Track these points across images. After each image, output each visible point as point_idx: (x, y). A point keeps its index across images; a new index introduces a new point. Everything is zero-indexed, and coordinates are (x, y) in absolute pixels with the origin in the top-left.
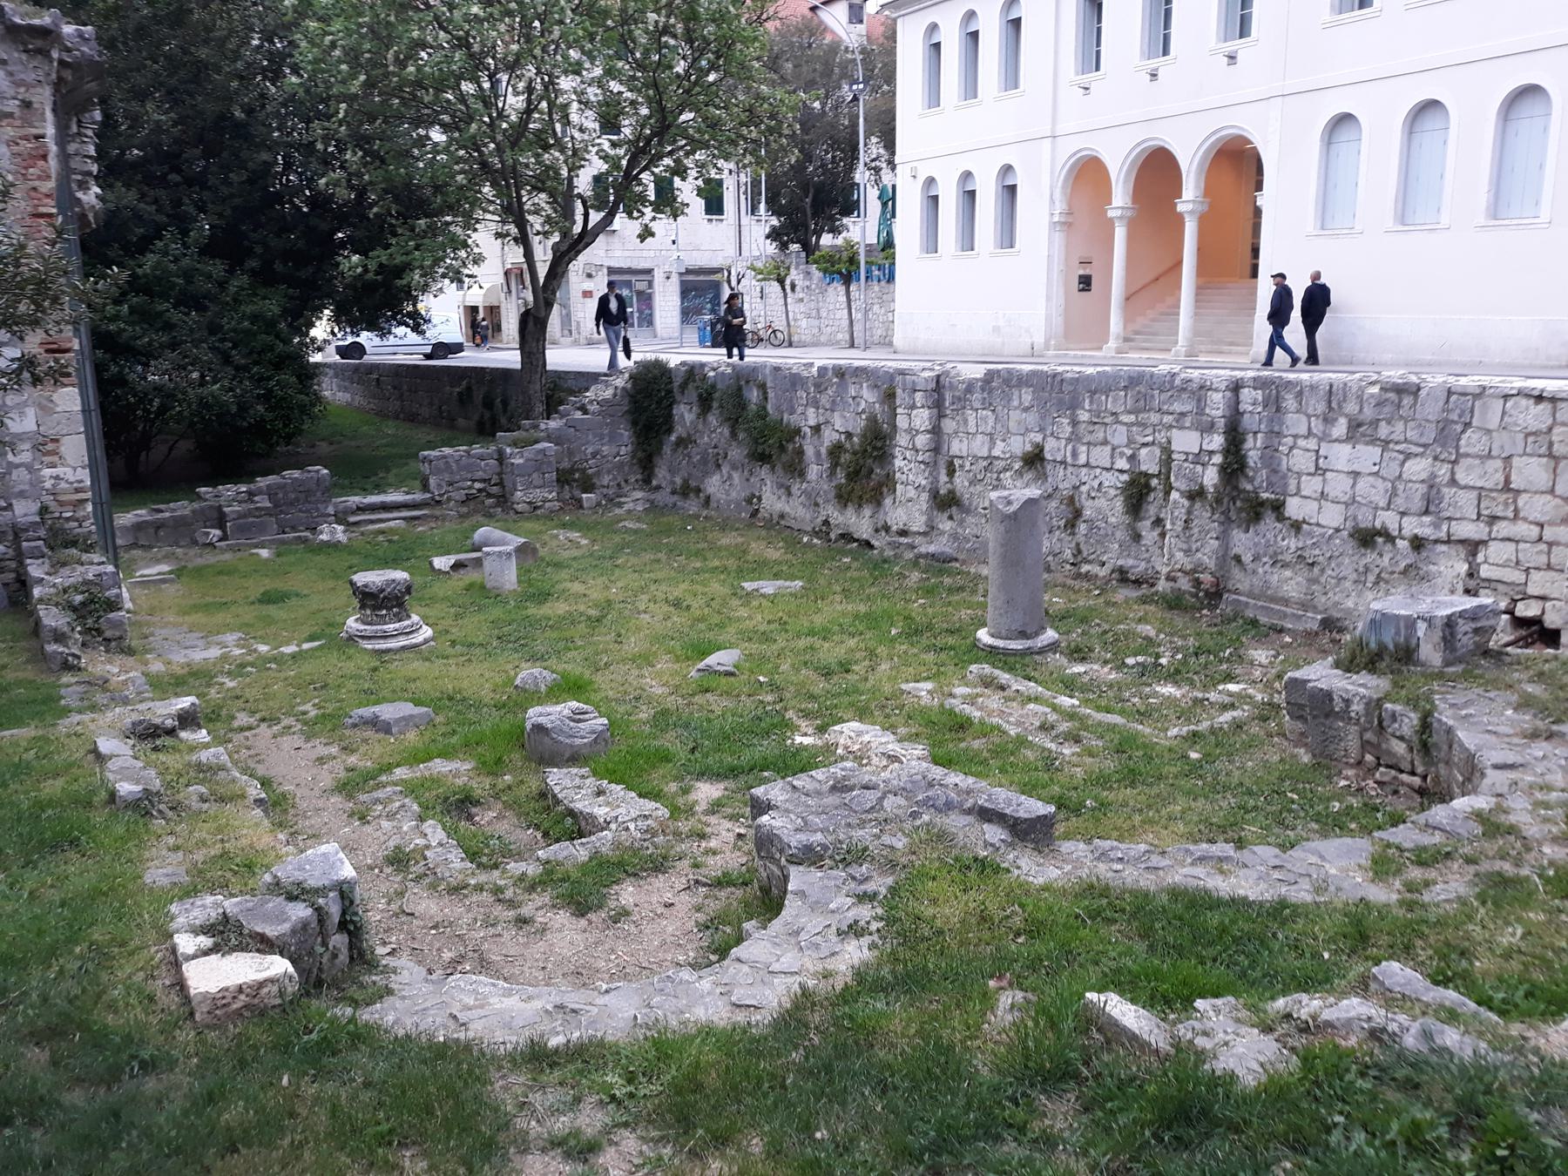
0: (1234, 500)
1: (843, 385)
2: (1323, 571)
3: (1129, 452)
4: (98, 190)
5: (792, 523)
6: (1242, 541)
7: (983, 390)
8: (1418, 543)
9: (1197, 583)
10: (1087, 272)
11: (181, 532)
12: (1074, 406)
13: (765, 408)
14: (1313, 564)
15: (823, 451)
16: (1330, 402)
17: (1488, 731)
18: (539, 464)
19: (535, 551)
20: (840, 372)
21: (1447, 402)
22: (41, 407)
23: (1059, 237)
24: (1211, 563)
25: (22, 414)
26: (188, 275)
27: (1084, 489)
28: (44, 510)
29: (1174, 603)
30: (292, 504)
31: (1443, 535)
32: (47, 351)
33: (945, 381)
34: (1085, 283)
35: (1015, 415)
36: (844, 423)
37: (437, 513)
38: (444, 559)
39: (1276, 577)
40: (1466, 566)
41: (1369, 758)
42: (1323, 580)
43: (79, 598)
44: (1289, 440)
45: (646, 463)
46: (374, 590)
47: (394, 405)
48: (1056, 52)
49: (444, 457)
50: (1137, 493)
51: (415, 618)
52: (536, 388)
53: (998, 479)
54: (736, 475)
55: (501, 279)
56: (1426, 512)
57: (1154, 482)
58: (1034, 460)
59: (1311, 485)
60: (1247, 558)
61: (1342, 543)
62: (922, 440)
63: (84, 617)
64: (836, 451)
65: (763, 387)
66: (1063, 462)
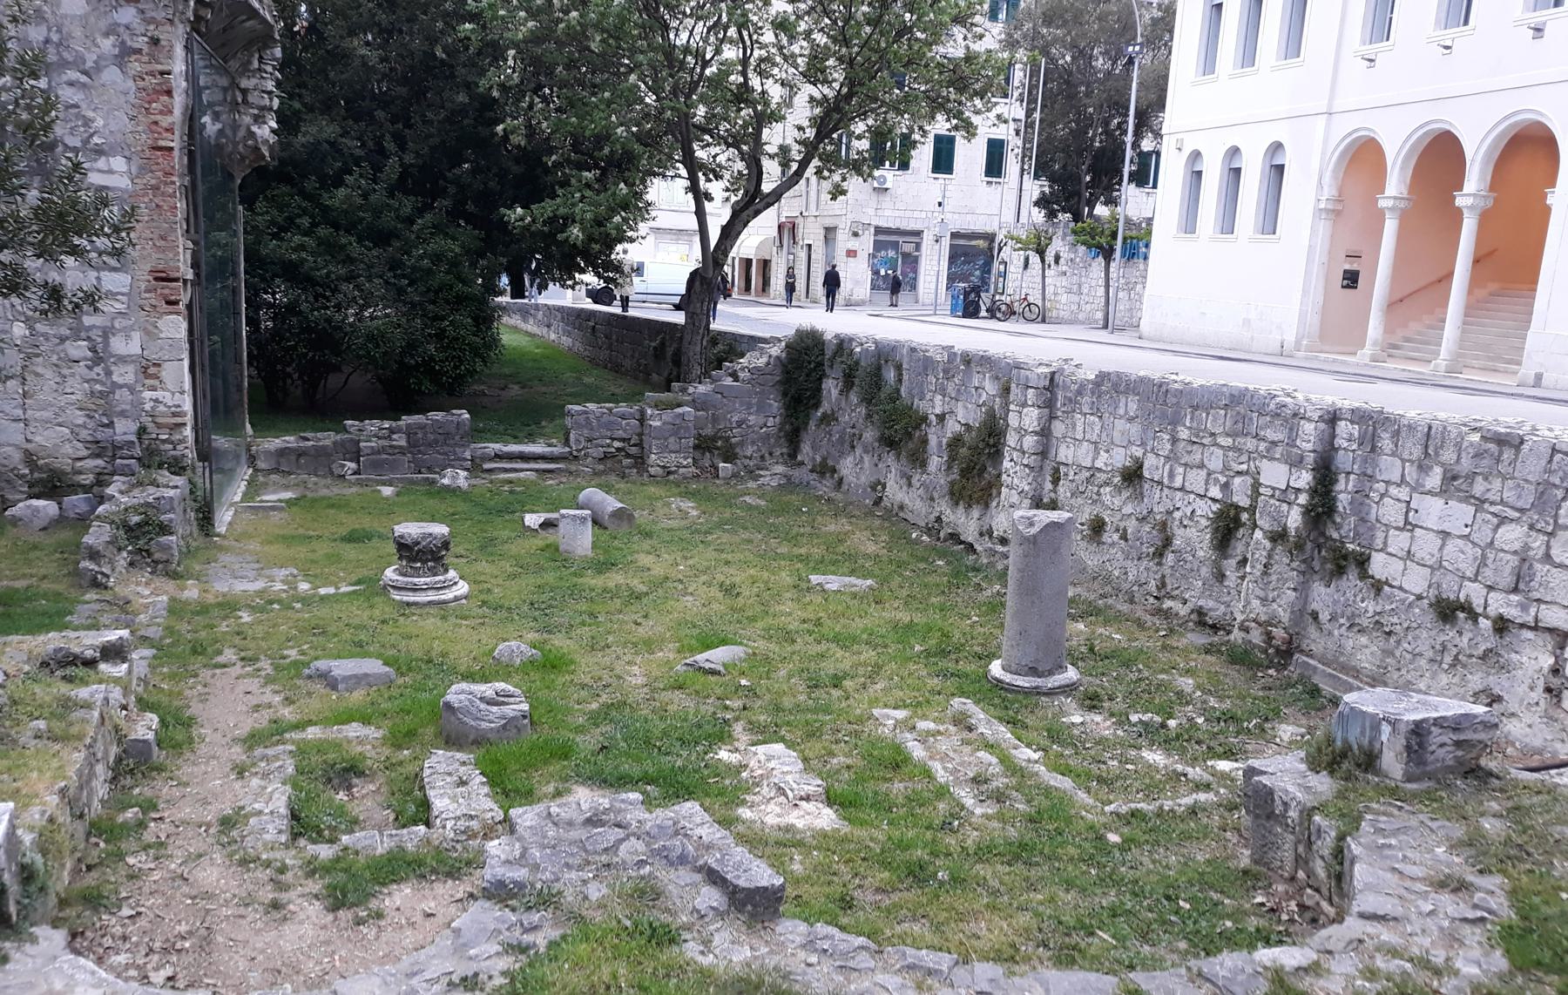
0: (1319, 547)
1: (968, 373)
2: (1398, 642)
3: (1223, 480)
4: (275, 125)
5: (909, 516)
6: (1322, 596)
7: (1093, 393)
8: (1502, 625)
9: (1269, 637)
10: (1355, 267)
11: (320, 461)
12: (1176, 421)
13: (898, 391)
14: (1389, 633)
15: (945, 441)
16: (1426, 447)
17: (1394, 869)
18: (676, 429)
19: (631, 517)
20: (967, 359)
21: (1550, 461)
22: (147, 332)
23: (1324, 228)
24: (1285, 616)
25: (128, 337)
26: (377, 212)
27: (1177, 515)
28: (142, 431)
29: (1240, 658)
30: (430, 445)
31: (1530, 619)
32: (156, 279)
33: (1059, 379)
34: (1351, 279)
35: (1120, 424)
36: (966, 415)
37: (573, 468)
38: (534, 516)
39: (1351, 642)
40: (1552, 661)
41: (1301, 874)
42: (1398, 654)
43: (136, 519)
44: (1381, 487)
45: (793, 437)
46: (409, 541)
47: (604, 354)
48: (1343, 20)
49: (586, 412)
50: (1228, 526)
51: (452, 574)
52: (695, 350)
53: (1098, 494)
54: (866, 458)
55: (775, 233)
56: (1515, 590)
57: (1245, 516)
58: (1133, 476)
59: (1398, 542)
60: (1324, 617)
61: (1422, 615)
62: (1030, 442)
63: (138, 538)
64: (956, 442)
65: (899, 367)
66: (1160, 483)
